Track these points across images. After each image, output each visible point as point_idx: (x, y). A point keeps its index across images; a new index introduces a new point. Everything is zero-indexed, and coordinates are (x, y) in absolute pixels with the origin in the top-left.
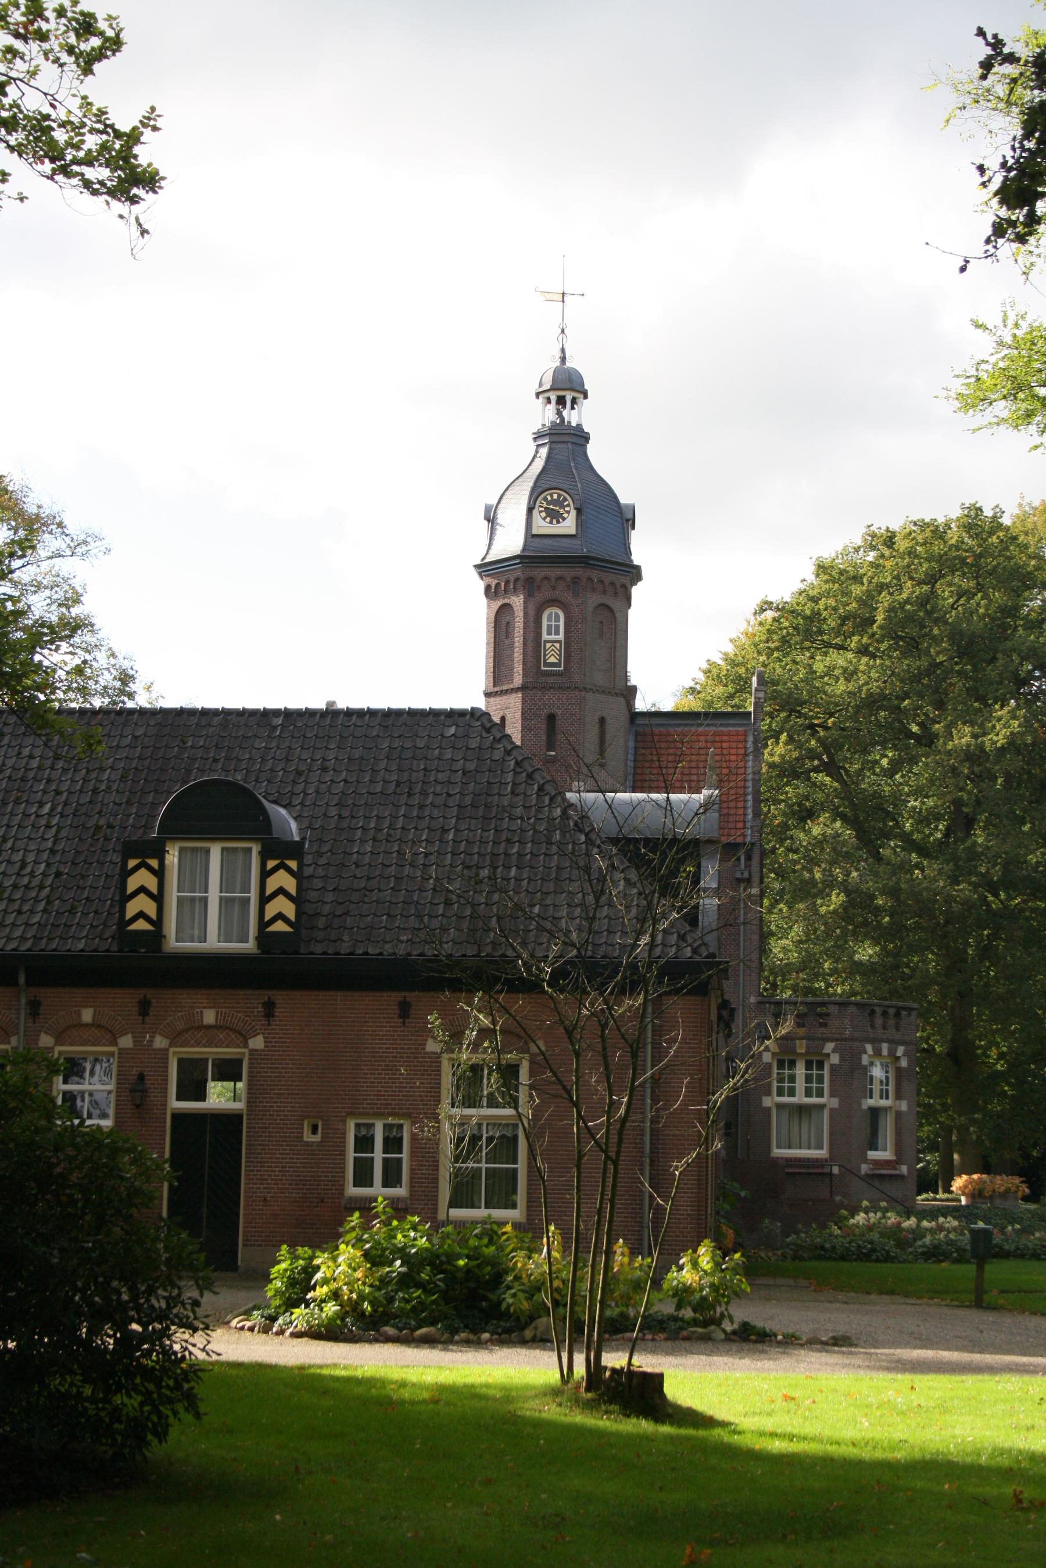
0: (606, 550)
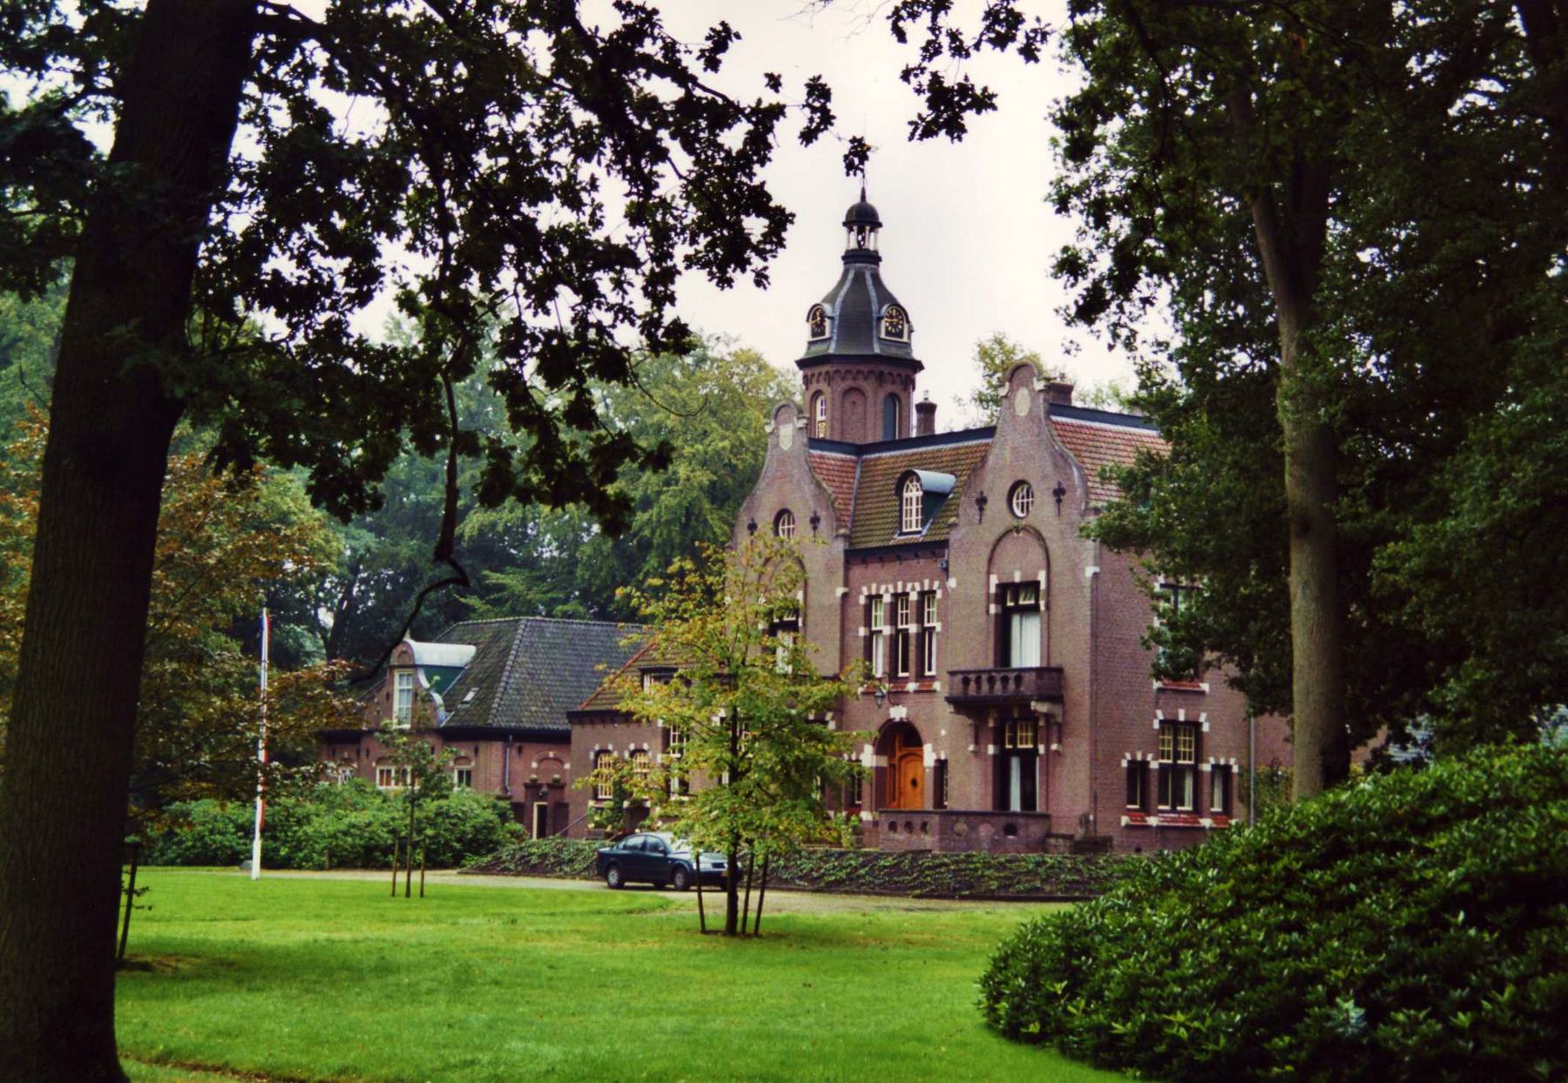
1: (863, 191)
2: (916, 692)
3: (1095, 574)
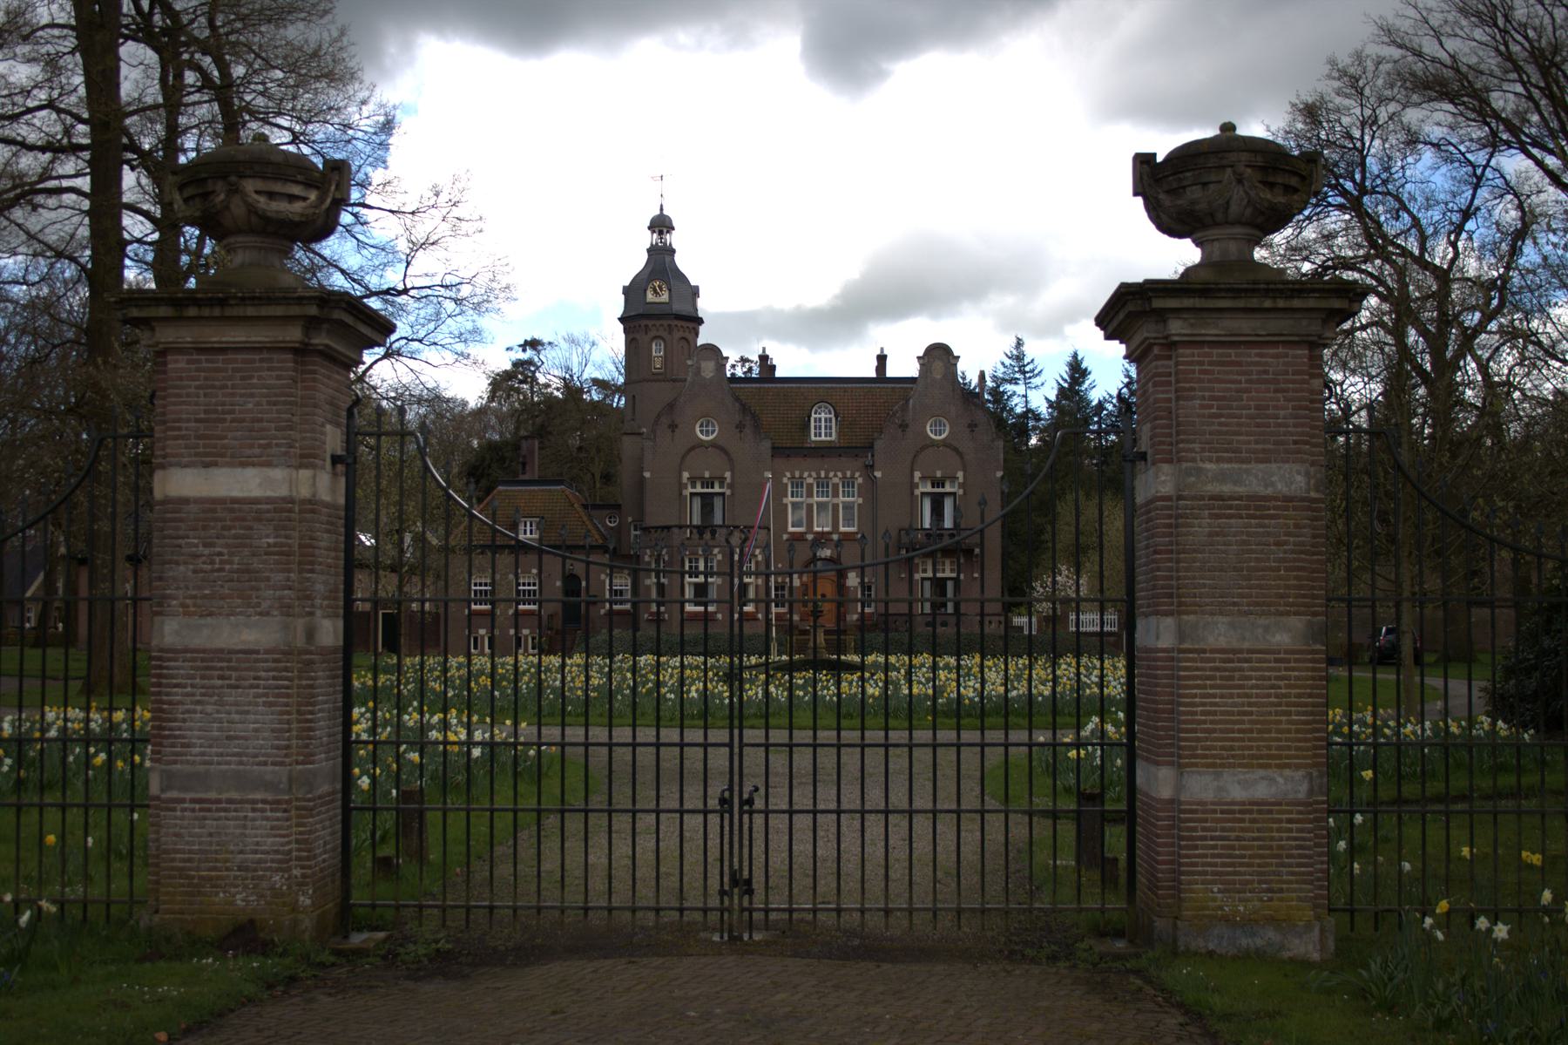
0: (678, 307)
1: (661, 225)
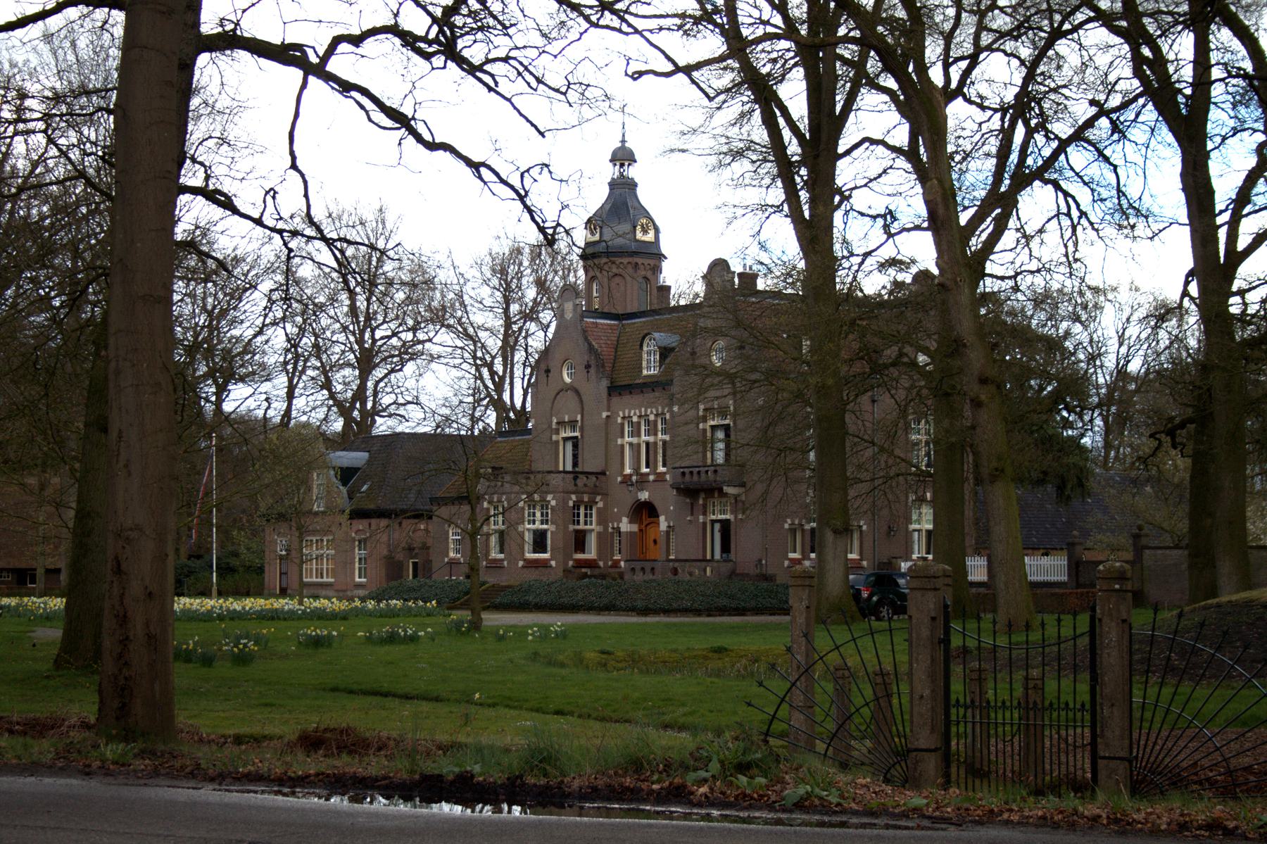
1: (623, 157)
2: (654, 481)
3: (608, 417)
